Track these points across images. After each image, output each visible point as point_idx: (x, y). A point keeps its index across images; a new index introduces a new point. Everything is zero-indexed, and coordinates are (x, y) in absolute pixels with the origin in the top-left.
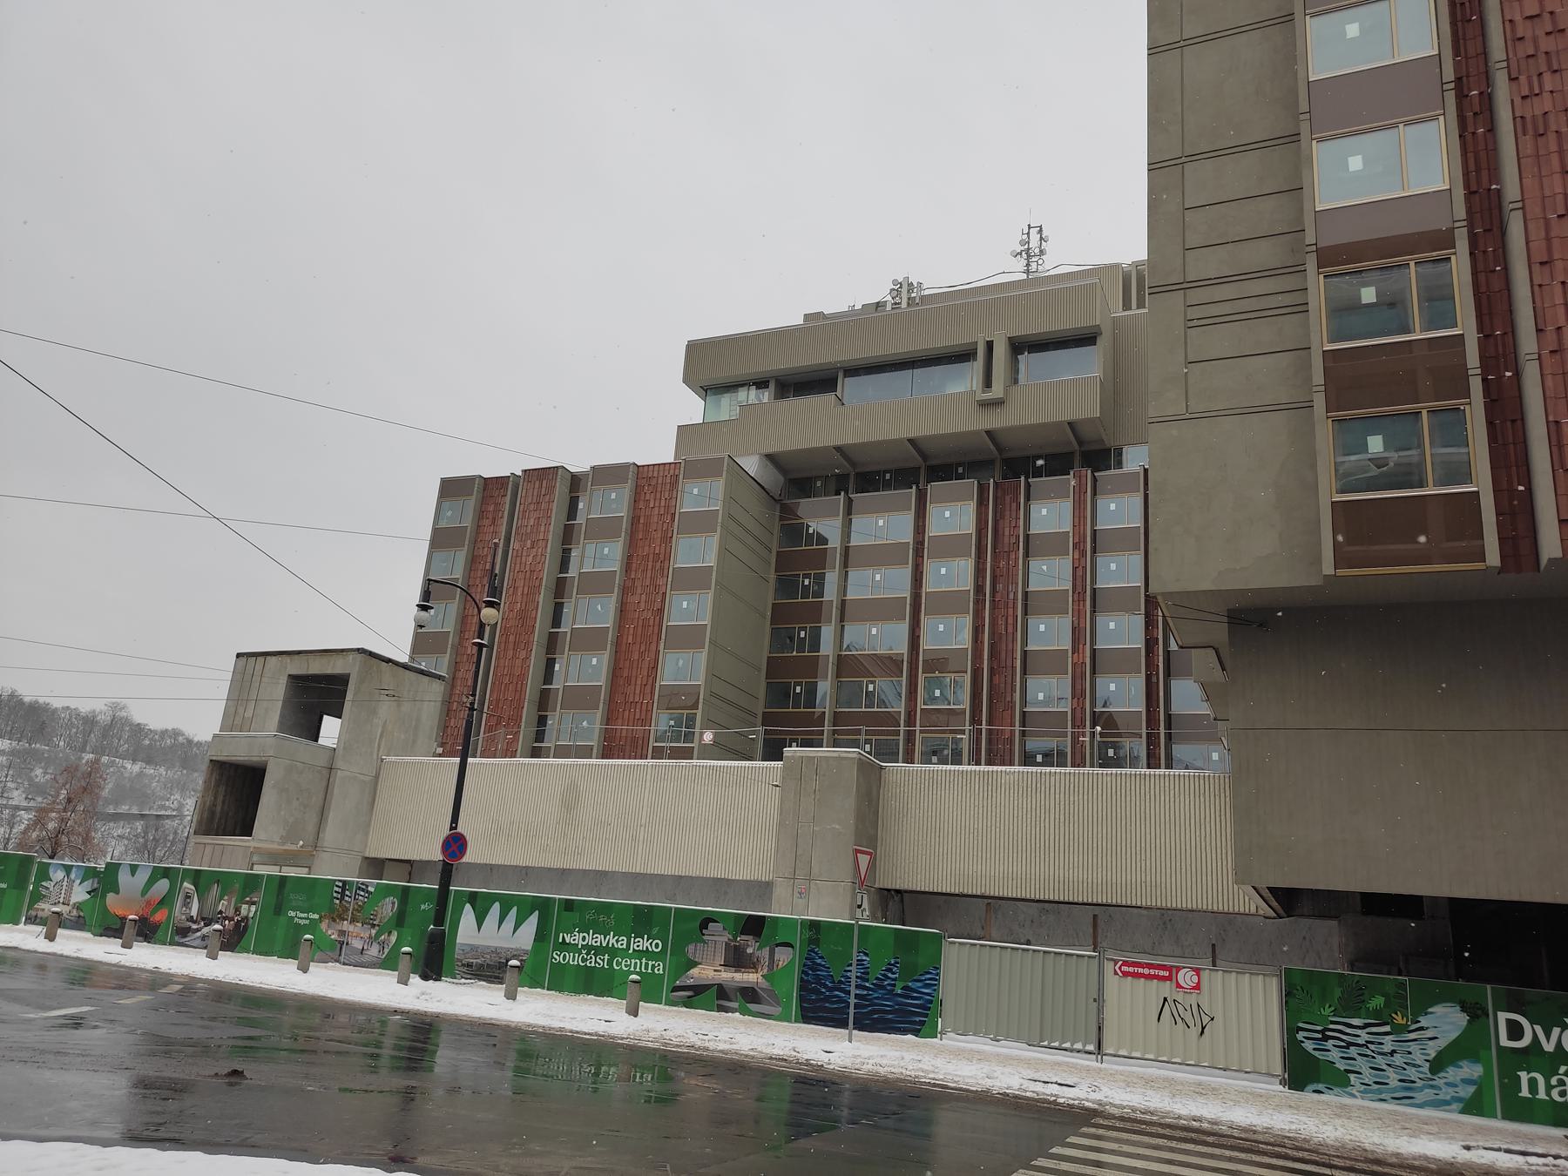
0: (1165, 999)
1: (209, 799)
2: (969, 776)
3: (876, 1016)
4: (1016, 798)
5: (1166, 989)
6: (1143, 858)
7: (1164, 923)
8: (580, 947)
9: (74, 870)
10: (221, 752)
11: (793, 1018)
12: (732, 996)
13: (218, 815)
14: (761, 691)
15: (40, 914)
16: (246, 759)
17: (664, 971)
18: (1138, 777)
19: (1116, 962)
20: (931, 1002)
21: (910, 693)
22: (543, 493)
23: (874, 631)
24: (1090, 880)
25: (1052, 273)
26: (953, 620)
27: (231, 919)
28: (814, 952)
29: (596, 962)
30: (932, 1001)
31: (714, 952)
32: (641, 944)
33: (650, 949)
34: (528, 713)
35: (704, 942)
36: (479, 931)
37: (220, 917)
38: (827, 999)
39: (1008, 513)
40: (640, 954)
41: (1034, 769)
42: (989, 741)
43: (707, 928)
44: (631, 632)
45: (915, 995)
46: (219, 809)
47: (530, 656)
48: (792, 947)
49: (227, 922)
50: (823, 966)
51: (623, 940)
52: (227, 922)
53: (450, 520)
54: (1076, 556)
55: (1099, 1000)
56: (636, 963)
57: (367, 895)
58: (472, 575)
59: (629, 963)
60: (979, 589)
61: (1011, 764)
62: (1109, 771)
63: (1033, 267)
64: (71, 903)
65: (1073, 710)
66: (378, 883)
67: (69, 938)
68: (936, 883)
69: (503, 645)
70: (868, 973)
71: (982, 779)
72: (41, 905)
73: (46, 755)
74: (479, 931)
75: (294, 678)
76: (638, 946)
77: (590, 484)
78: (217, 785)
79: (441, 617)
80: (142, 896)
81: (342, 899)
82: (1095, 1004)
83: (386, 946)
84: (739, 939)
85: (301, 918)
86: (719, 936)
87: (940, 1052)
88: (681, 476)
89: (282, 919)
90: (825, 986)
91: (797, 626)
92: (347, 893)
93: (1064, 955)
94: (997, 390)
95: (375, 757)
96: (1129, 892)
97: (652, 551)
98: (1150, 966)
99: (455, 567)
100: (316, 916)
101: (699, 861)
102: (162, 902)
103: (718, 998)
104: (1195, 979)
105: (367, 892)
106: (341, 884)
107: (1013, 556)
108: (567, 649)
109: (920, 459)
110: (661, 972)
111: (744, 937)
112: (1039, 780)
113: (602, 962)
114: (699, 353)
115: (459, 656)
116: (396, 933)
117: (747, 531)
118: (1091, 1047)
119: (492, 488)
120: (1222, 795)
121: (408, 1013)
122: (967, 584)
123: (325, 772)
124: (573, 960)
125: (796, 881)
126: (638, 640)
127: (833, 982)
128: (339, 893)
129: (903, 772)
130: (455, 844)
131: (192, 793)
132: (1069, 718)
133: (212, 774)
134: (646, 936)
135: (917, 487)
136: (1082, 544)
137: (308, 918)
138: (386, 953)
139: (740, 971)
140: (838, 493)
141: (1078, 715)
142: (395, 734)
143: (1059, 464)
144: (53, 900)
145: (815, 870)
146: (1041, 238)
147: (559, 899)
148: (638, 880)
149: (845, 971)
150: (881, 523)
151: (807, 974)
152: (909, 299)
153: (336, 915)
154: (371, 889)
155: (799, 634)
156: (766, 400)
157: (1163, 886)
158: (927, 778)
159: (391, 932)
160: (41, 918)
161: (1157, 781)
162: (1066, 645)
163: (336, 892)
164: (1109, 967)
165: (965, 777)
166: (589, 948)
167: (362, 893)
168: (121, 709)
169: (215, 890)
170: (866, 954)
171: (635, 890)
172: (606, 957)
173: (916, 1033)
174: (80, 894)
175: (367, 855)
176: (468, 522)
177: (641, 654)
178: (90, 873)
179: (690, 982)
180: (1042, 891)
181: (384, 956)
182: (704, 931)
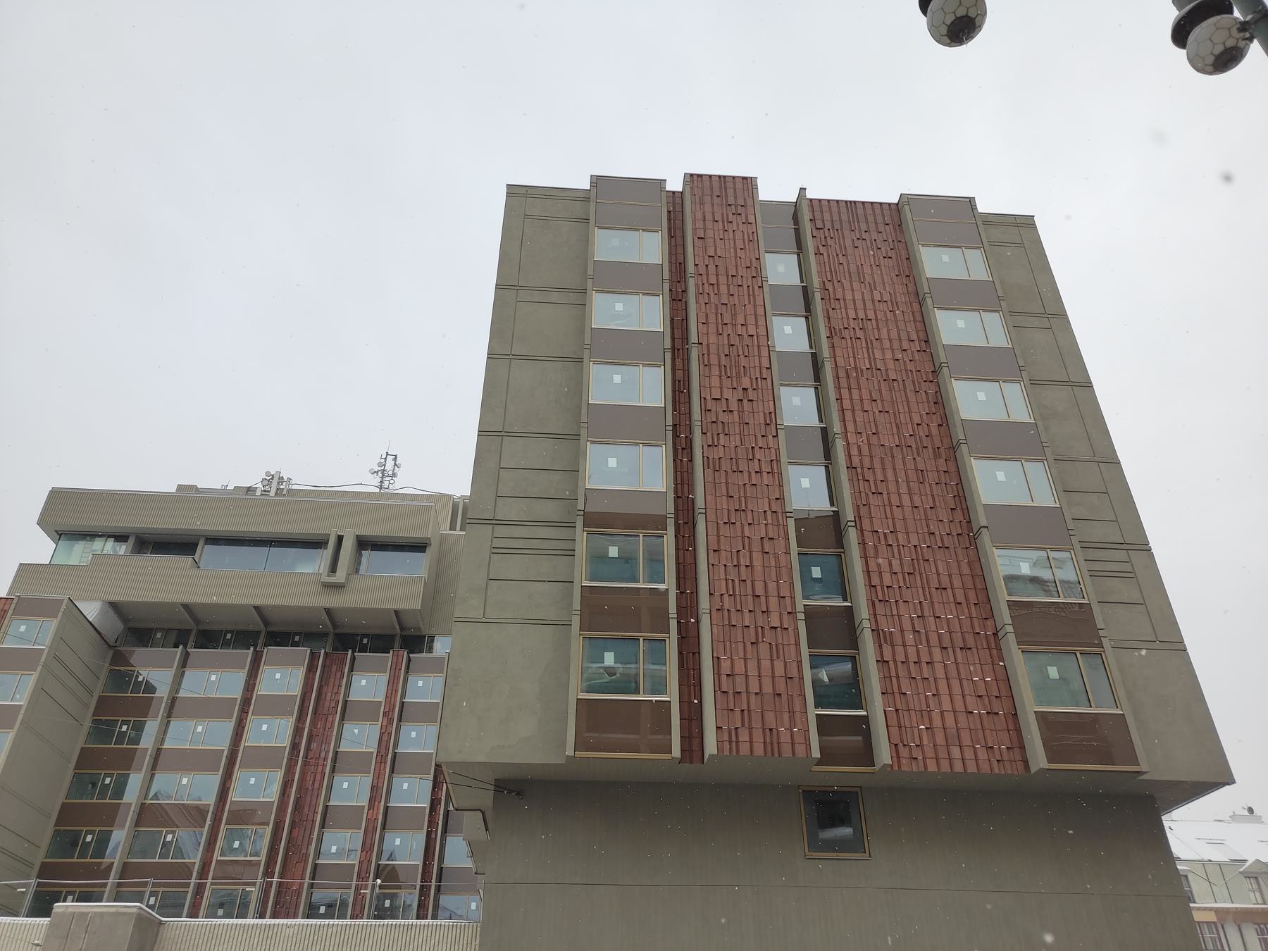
26: (265, 773)
39: (332, 680)
42: (278, 893)
54: (385, 724)
60: (295, 746)
63: (386, 484)
65: (361, 863)
88: (10, 612)
94: (340, 576)
109: (192, 622)
136: (391, 713)
143: (381, 643)
146: (395, 464)
156: (122, 553)
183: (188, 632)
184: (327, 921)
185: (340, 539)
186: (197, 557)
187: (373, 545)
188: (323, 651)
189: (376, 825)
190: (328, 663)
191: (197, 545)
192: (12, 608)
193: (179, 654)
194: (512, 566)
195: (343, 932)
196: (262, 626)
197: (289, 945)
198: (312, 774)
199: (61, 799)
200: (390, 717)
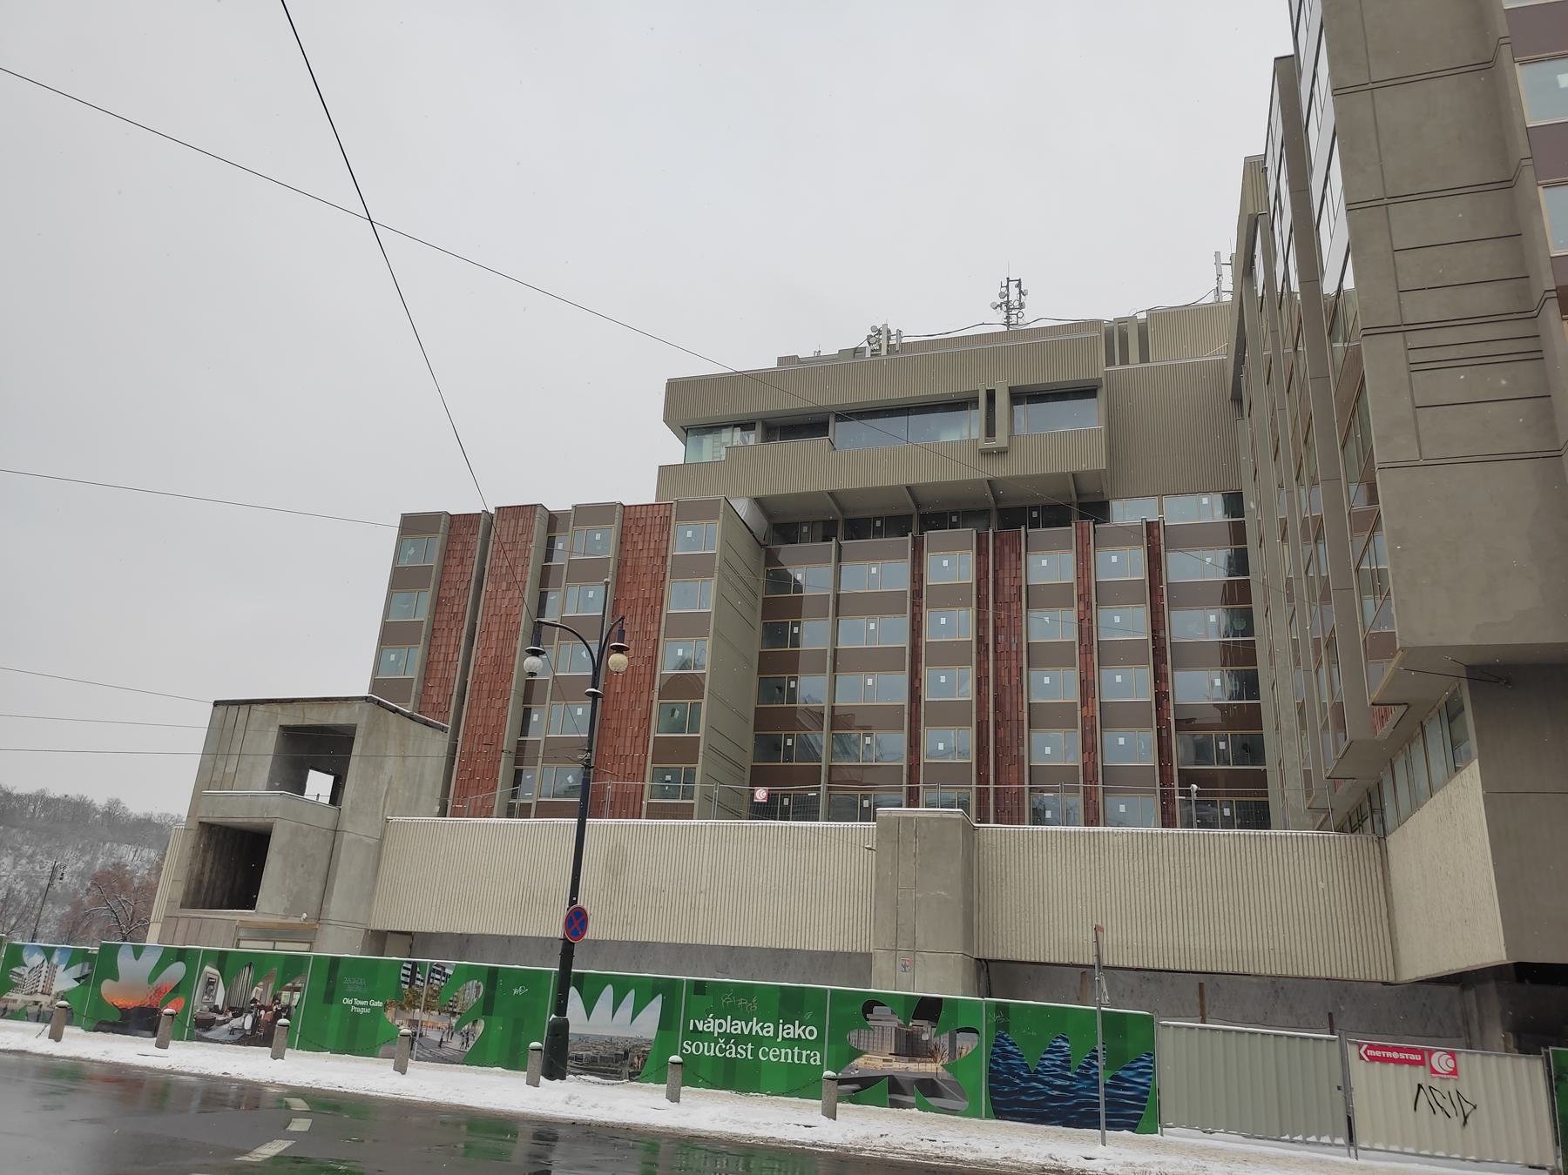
0: (1420, 1086)
1: (197, 867)
2: (1073, 837)
3: (1083, 1110)
4: (1126, 861)
5: (1420, 1074)
6: (1269, 923)
7: (1276, 992)
8: (716, 1035)
9: (57, 953)
10: (213, 812)
13: (206, 885)
15: (11, 1006)
16: (246, 820)
17: (822, 1060)
18: (1258, 839)
19: (1360, 1046)
20: (1147, 1093)
21: (911, 746)
23: (870, 682)
24: (1213, 948)
25: (1031, 326)
27: (267, 1009)
28: (1003, 1038)
29: (737, 1052)
30: (1148, 1092)
31: (882, 1039)
32: (792, 1031)
33: (803, 1037)
34: (505, 766)
35: (869, 1028)
36: (588, 1019)
37: (253, 1006)
38: (1024, 1091)
39: (1007, 563)
40: (792, 1042)
42: (996, 798)
43: (872, 1013)
44: (620, 680)
45: (1127, 1085)
46: (206, 878)
48: (977, 1033)
49: (263, 1012)
50: (1015, 1053)
51: (769, 1027)
52: (263, 1012)
54: (1082, 608)
55: (1346, 1088)
56: (786, 1053)
57: (443, 978)
59: (778, 1053)
60: (981, 640)
61: (1020, 821)
62: (1247, 832)
63: (1014, 319)
64: (53, 992)
65: (1085, 765)
66: (457, 964)
68: (1042, 952)
71: (1087, 841)
72: (12, 995)
74: (588, 1019)
75: (284, 728)
76: (788, 1034)
77: (571, 523)
79: (402, 662)
80: (149, 983)
81: (411, 984)
82: (1341, 1093)
83: (470, 1037)
84: (911, 1024)
85: (360, 1006)
86: (887, 1022)
87: (1166, 1148)
88: (673, 518)
90: (1020, 1077)
91: (787, 676)
92: (419, 976)
93: (1272, 1036)
94: (1001, 440)
95: (381, 818)
96: (1256, 961)
97: (641, 595)
98: (1399, 1050)
99: (420, 608)
100: (380, 1004)
101: (770, 931)
102: (176, 989)
103: (892, 1092)
104: (1451, 1063)
105: (444, 974)
106: (410, 966)
107: (1014, 607)
109: (838, 512)
110: (818, 1063)
111: (917, 1022)
112: (1150, 841)
113: (745, 1052)
114: (678, 391)
115: (422, 706)
117: (741, 578)
118: (1340, 1141)
119: (459, 526)
120: (1350, 858)
121: (589, 1125)
123: (330, 834)
124: (708, 1050)
125: (899, 952)
126: (628, 689)
127: (1029, 1072)
128: (408, 976)
129: (999, 833)
130: (577, 920)
131: (10, 851)
132: (1081, 773)
133: (200, 838)
134: (797, 1022)
136: (1087, 596)
137: (368, 1006)
138: (471, 1046)
139: (915, 1061)
140: (826, 538)
141: (1090, 770)
142: (400, 791)
143: (1055, 515)
144: (28, 989)
145: (920, 941)
146: (1021, 292)
147: (687, 980)
148: (781, 958)
149: (1042, 1059)
150: (874, 570)
151: (998, 1064)
152: (888, 346)
153: (406, 1002)
155: (789, 684)
156: (752, 442)
157: (1294, 953)
158: (1026, 839)
160: (12, 1011)
161: (1279, 843)
162: (1075, 698)
163: (403, 975)
164: (1352, 1051)
165: (1068, 838)
166: (728, 1037)
167: (438, 976)
170: (1066, 1040)
171: (681, 962)
172: (750, 1046)
173: (1133, 1128)
174: (65, 981)
175: (372, 927)
176: (434, 561)
179: (855, 1074)
180: (1161, 959)
181: (469, 1049)
182: (868, 1016)
185: (991, 396)
187: (1028, 396)
190: (998, 544)
192: (674, 513)
194: (1456, 383)
195: (1181, 842)
197: (1121, 854)
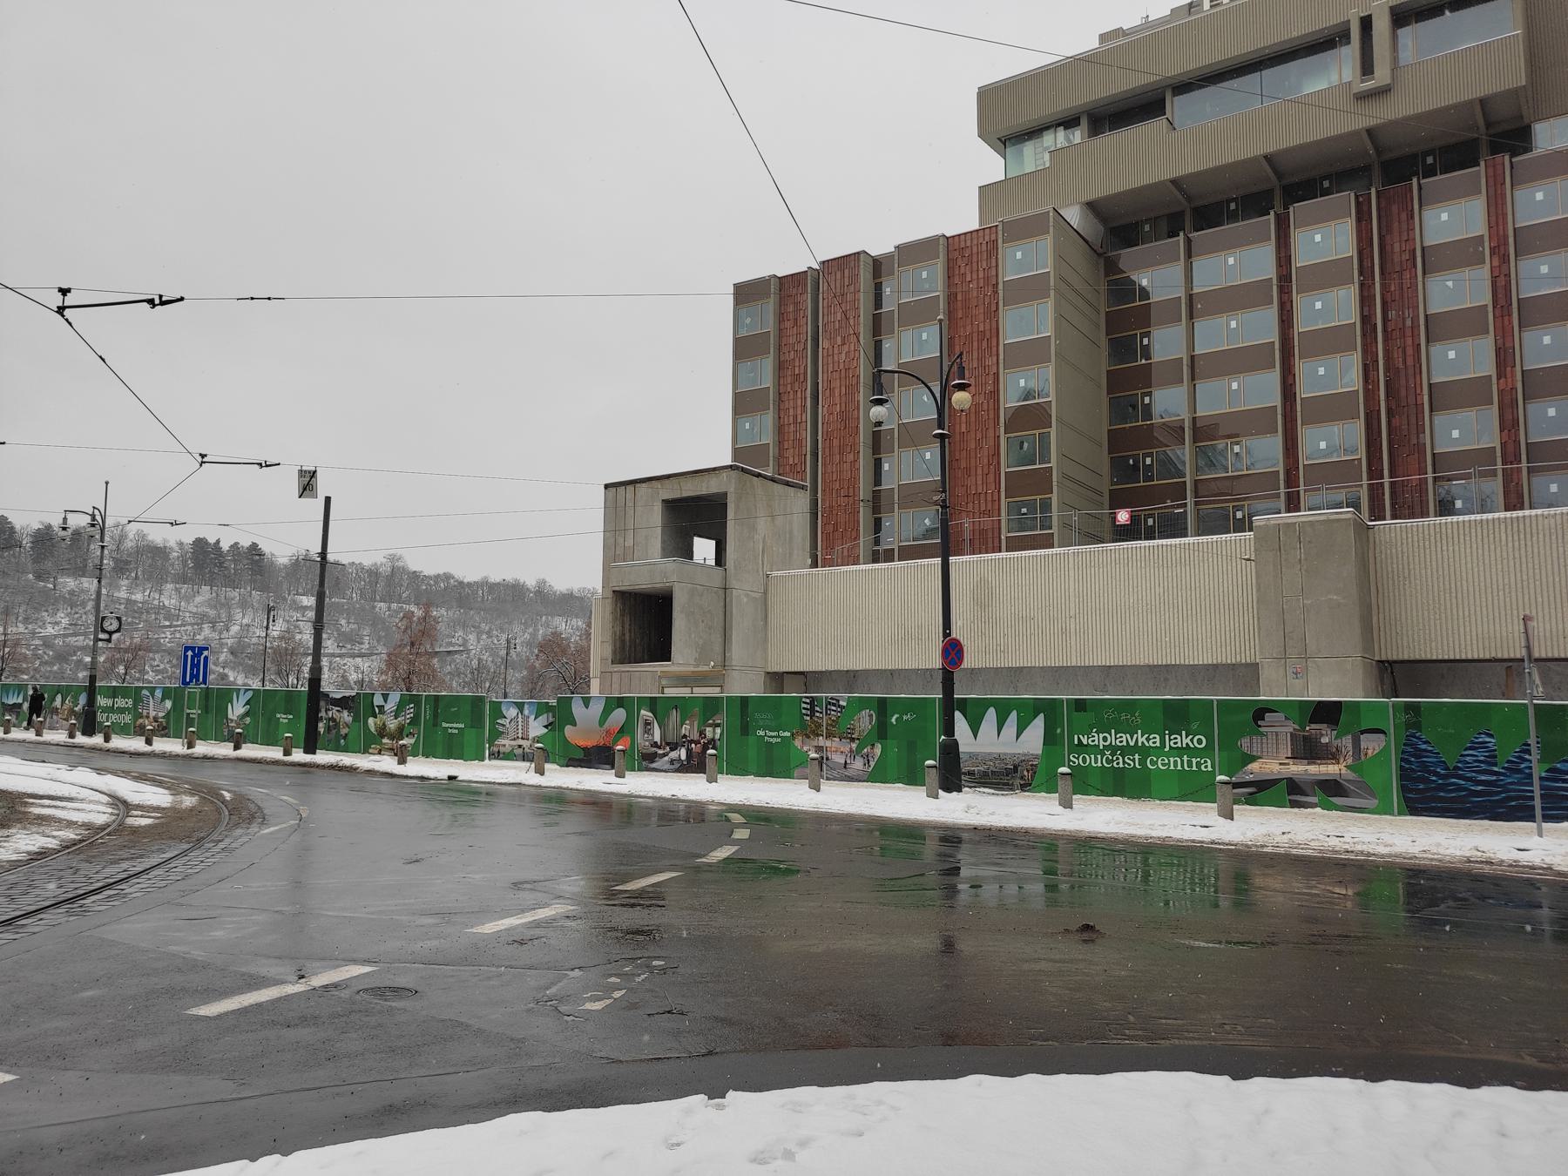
1: (618, 629)
8: (1101, 747)
9: (526, 706)
11: (1396, 811)
12: (1308, 791)
14: (1105, 469)
16: (649, 586)
22: (847, 283)
26: (1337, 360)
27: (697, 743)
28: (1415, 737)
29: (1124, 762)
34: (864, 516)
35: (1262, 734)
36: (1017, 739)
37: (683, 741)
38: (1441, 788)
39: (1396, 225)
40: (1180, 751)
41: (1455, 518)
44: (964, 418)
47: (858, 458)
48: (1383, 732)
49: (693, 745)
50: (1430, 751)
53: (750, 328)
54: (1496, 263)
57: (839, 709)
58: (782, 382)
59: (1167, 761)
60: (1367, 320)
61: (1424, 514)
64: (530, 738)
65: (1504, 445)
67: (322, 753)
69: (827, 450)
70: (1496, 757)
73: (346, 607)
74: (1017, 739)
77: (896, 265)
78: (622, 615)
84: (1308, 728)
85: (772, 737)
88: (1000, 241)
89: (751, 739)
91: (1139, 392)
95: (761, 574)
99: (764, 374)
100: (787, 734)
102: (622, 730)
105: (839, 706)
106: (808, 701)
108: (896, 447)
110: (1210, 769)
111: (1313, 726)
113: (1134, 761)
116: (880, 746)
117: (1075, 291)
119: (788, 287)
121: (990, 829)
122: (1352, 315)
123: (721, 592)
124: (1093, 761)
127: (1447, 769)
128: (808, 703)
130: (953, 651)
135: (1185, 234)
138: (872, 767)
139: (1315, 763)
140: (1173, 234)
144: (512, 735)
149: (1462, 755)
151: (1410, 762)
153: (811, 732)
154: (843, 703)
159: (873, 745)
160: (504, 753)
163: (804, 708)
166: (1114, 749)
167: (834, 708)
168: (397, 560)
169: (674, 716)
170: (1491, 736)
172: (1137, 756)
174: (537, 728)
175: (769, 670)
176: (770, 326)
177: (978, 442)
178: (542, 709)
181: (871, 769)
182: (1259, 723)
183: (1181, 214)
184: (1467, 518)
185: (1366, 23)
186: (1168, 114)
188: (1373, 191)
189: (1514, 396)
191: (1163, 100)
193: (1272, 221)
196: (1186, 203)
198: (1400, 349)
199: (1105, 428)
200: (1502, 252)
